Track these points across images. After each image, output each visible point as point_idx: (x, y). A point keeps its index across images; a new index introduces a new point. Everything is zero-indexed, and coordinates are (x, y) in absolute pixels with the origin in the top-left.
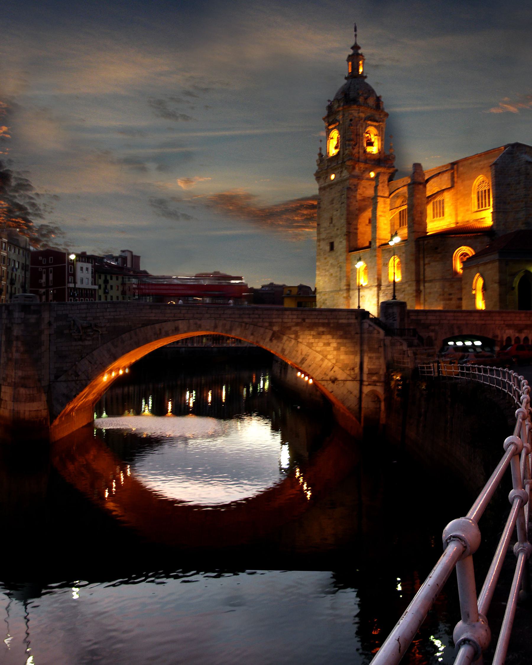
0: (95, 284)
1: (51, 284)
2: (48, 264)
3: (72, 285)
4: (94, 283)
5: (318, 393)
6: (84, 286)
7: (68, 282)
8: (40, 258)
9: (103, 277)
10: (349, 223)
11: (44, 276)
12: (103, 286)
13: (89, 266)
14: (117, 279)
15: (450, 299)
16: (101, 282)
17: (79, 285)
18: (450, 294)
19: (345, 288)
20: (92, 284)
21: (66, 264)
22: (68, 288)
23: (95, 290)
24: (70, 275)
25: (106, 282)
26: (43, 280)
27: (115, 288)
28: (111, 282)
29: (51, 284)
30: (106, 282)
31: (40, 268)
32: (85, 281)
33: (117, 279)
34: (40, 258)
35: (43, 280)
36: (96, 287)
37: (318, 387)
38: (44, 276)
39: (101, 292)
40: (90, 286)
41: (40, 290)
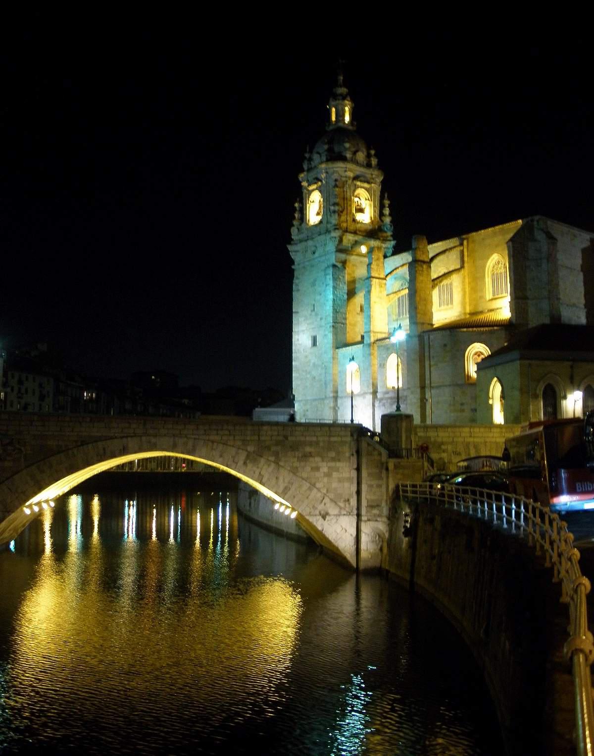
15: (463, 411)
18: (462, 404)
19: (331, 395)
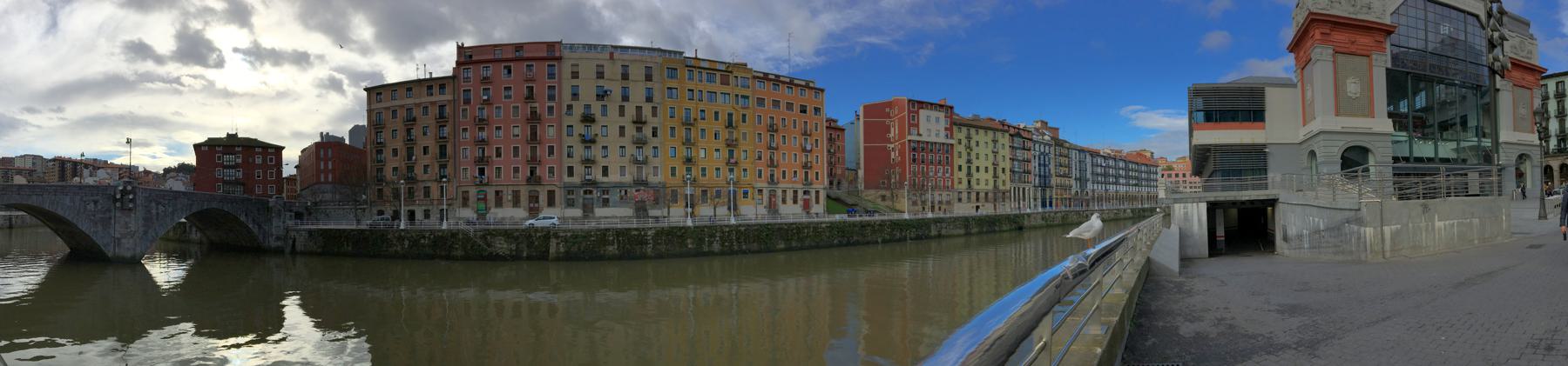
6: (933, 139)
13: (942, 115)
25: (969, 138)
28: (975, 138)
30: (969, 138)
39: (961, 148)
40: (942, 139)
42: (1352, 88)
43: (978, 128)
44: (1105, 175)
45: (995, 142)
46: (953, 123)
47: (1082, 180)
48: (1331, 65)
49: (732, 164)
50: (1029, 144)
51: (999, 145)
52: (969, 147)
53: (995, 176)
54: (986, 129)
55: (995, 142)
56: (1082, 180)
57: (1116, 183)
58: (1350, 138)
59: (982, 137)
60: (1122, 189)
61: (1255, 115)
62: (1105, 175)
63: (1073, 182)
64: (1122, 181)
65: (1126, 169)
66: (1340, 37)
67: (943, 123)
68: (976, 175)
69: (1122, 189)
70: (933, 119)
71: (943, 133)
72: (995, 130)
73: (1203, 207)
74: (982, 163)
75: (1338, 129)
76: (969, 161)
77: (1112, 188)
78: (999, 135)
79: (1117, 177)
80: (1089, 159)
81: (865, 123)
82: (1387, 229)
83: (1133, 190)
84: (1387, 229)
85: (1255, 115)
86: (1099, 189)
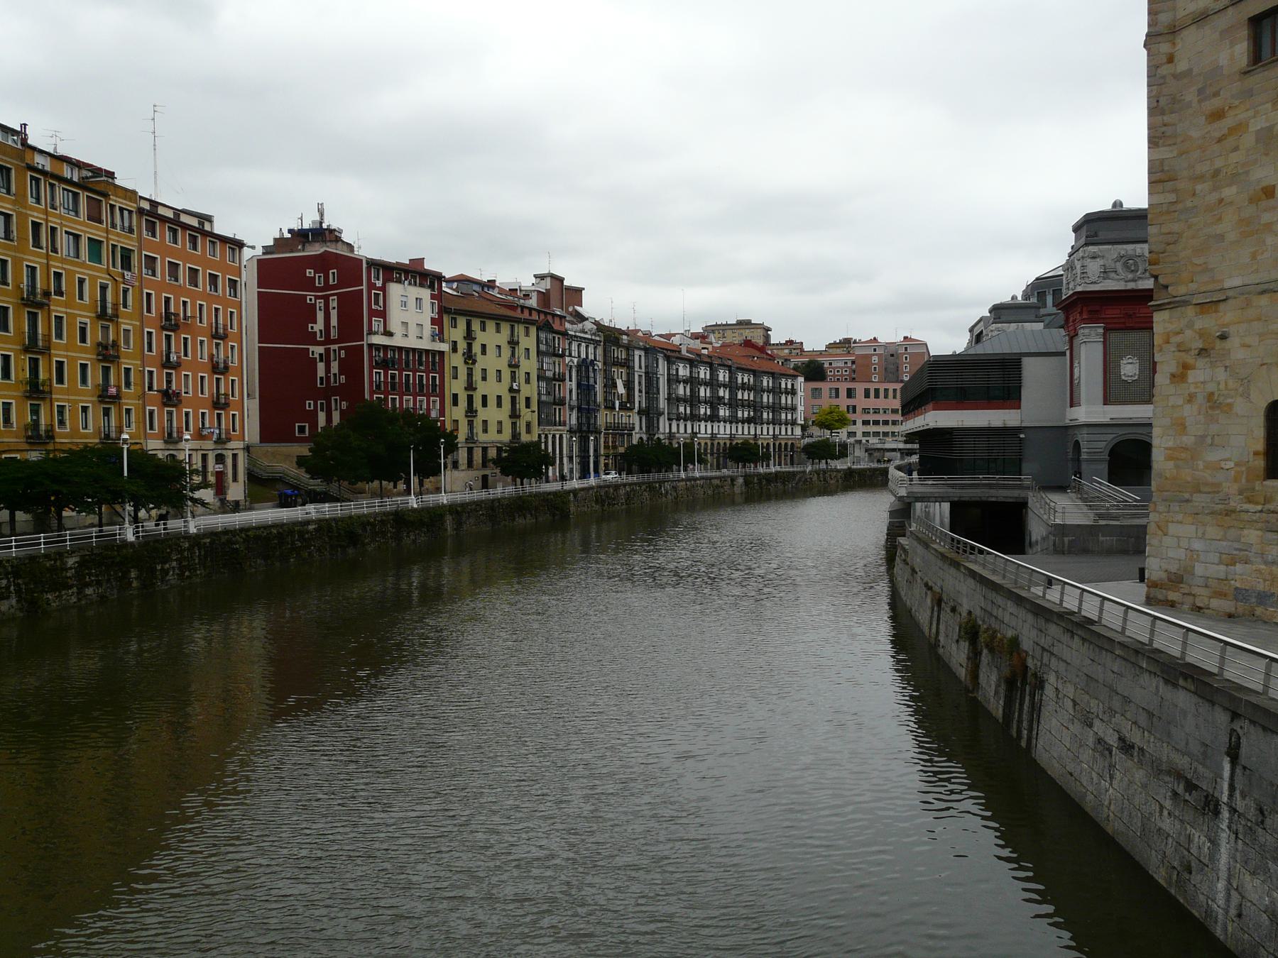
0: (442, 340)
1: (334, 334)
2: (327, 287)
3: (378, 340)
4: (439, 336)
5: (588, 325)
6: (412, 343)
7: (371, 332)
8: (310, 273)
9: (462, 322)
10: (472, 432)
11: (320, 316)
12: (462, 346)
13: (425, 294)
14: (498, 331)
16: (458, 334)
17: (398, 341)
20: (434, 340)
21: (364, 287)
22: (370, 346)
23: (442, 353)
24: (373, 313)
25: (469, 336)
26: (319, 326)
27: (491, 350)
28: (481, 338)
29: (334, 334)
30: (469, 336)
31: (310, 297)
32: (413, 331)
33: (498, 331)
34: (310, 273)
35: (319, 326)
36: (444, 347)
37: (1018, 644)
38: (320, 316)
39: (457, 360)
40: (425, 344)
41: (312, 348)
42: (1129, 369)
43: (484, 317)
44: (693, 400)
45: (513, 343)
46: (443, 310)
47: (650, 413)
48: (1100, 347)
49: (107, 398)
50: (562, 344)
51: (520, 351)
52: (469, 357)
53: (514, 415)
54: (498, 319)
55: (513, 343)
56: (650, 413)
57: (714, 418)
58: (1116, 430)
59: (491, 336)
60: (724, 430)
61: (1009, 395)
62: (693, 400)
63: (635, 419)
64: (723, 412)
65: (732, 386)
66: (1113, 312)
67: (428, 313)
68: (482, 414)
69: (724, 430)
70: (412, 303)
71: (428, 328)
72: (513, 321)
73: (946, 507)
74: (490, 388)
75: (1106, 420)
76: (470, 387)
77: (704, 429)
78: (520, 329)
79: (714, 402)
80: (662, 367)
81: (264, 302)
82: (1066, 539)
83: (744, 432)
84: (1066, 539)
85: (1009, 395)
86: (682, 430)
